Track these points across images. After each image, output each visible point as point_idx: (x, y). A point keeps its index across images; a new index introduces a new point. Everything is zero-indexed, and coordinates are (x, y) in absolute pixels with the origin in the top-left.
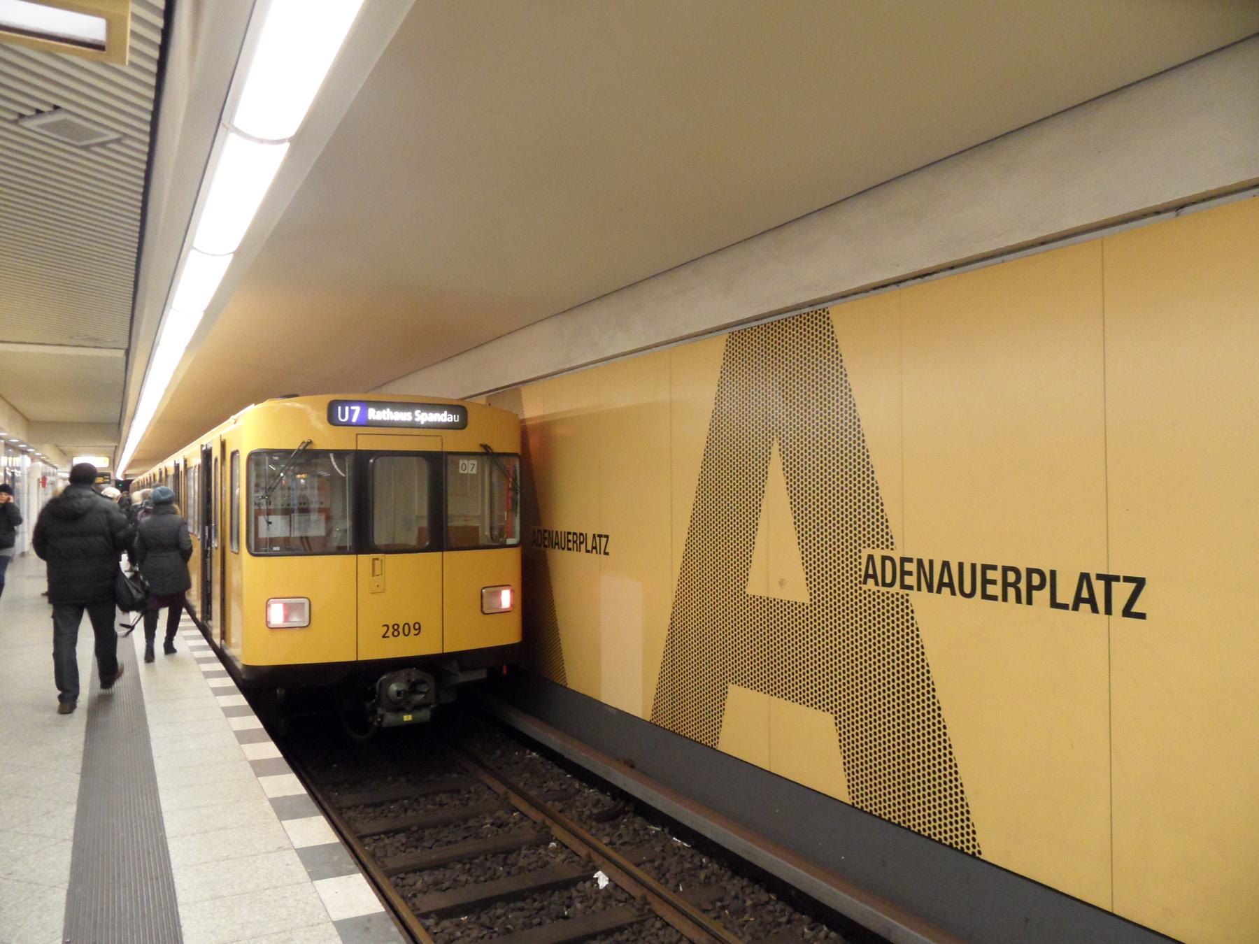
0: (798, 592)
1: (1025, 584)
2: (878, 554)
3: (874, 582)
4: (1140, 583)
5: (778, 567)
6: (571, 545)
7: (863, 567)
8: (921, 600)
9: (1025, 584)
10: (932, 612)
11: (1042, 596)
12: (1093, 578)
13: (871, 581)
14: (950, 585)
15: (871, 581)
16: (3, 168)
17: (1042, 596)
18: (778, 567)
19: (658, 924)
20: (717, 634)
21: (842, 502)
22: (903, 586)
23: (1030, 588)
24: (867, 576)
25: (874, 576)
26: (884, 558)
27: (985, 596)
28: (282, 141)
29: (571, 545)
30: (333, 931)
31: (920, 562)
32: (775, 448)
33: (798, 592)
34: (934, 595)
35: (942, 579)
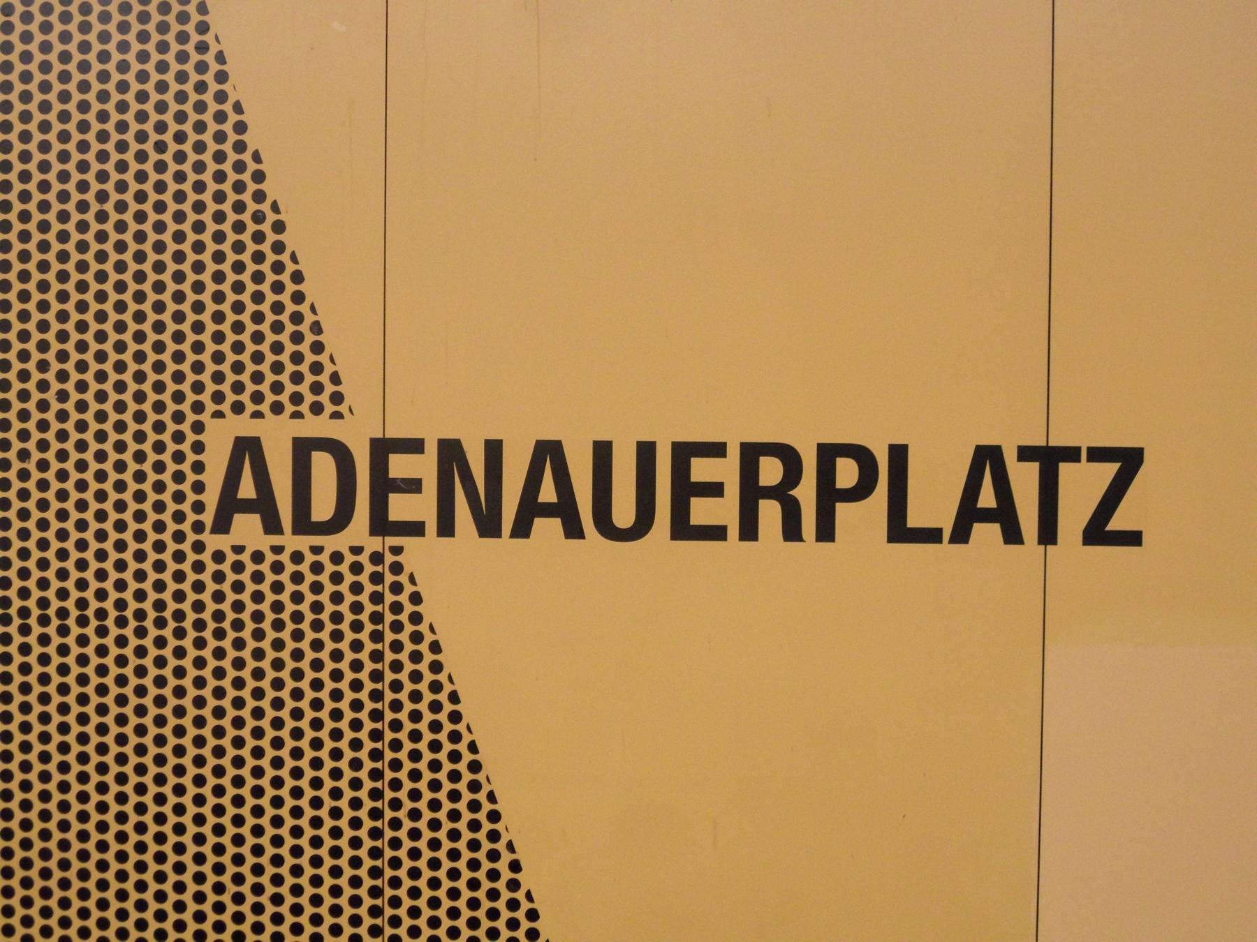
2: (279, 440)
4: (1129, 461)
7: (214, 479)
10: (463, 583)
13: (247, 528)
14: (565, 510)
15: (247, 528)
22: (380, 524)
23: (829, 496)
24: (230, 506)
25: (265, 506)
26: (303, 449)
27: (682, 529)
31: (451, 452)
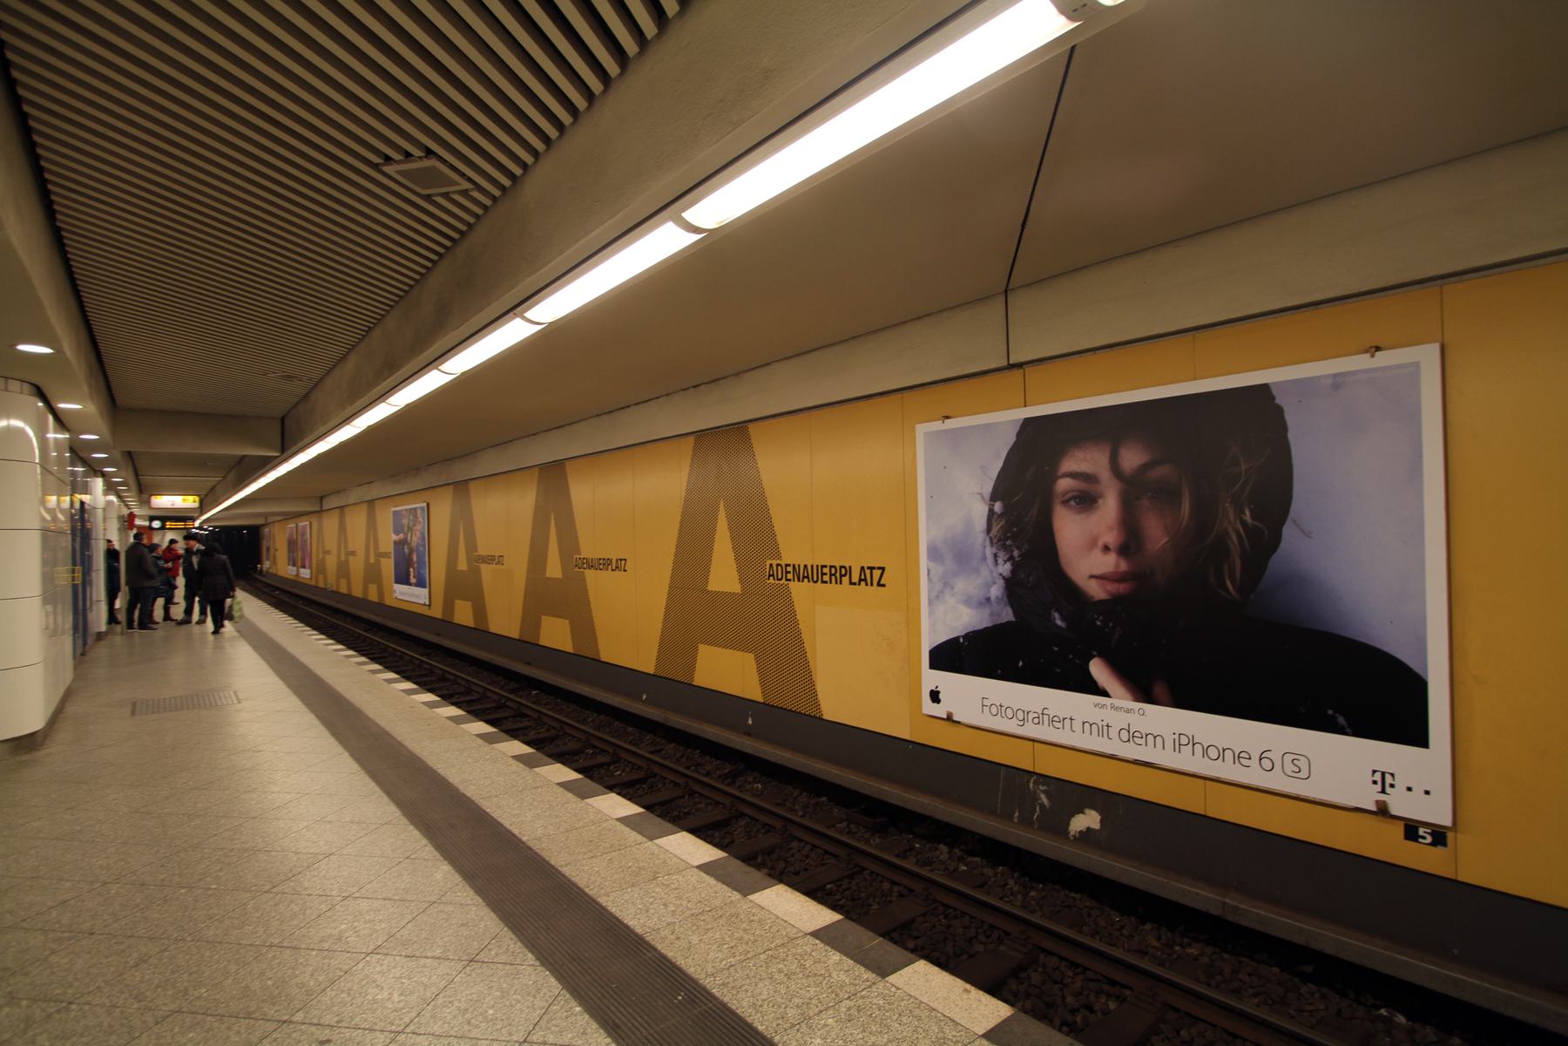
0: (736, 588)
1: (839, 574)
2: (774, 563)
3: (772, 578)
4: (883, 569)
5: (724, 576)
6: (826, 578)
8: (795, 587)
9: (839, 574)
10: (590, 574)
11: (846, 579)
12: (124, 624)
16: (7, 19)
17: (846, 579)
18: (724, 576)
19: (808, 848)
20: (692, 614)
21: (756, 536)
28: (696, 230)
29: (826, 578)
30: (984, 1042)
32: (49, 351)
33: (736, 588)
34: (137, 632)
35: (593, 565)
